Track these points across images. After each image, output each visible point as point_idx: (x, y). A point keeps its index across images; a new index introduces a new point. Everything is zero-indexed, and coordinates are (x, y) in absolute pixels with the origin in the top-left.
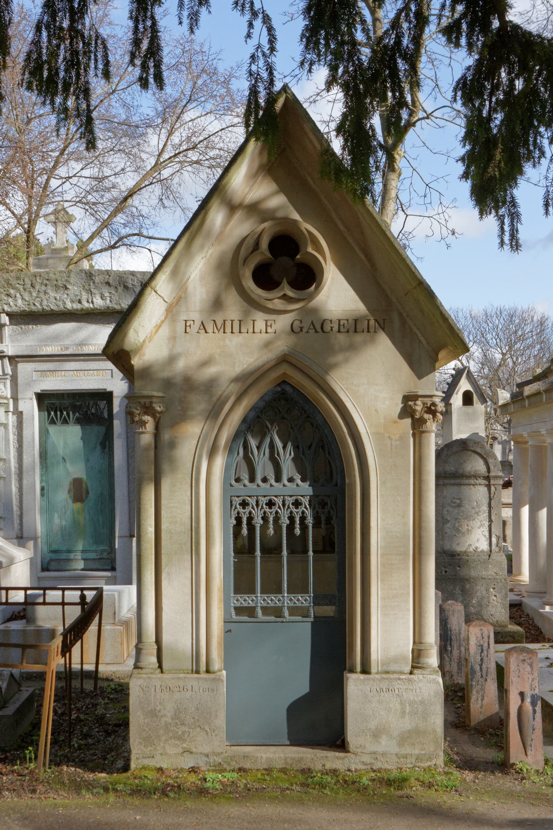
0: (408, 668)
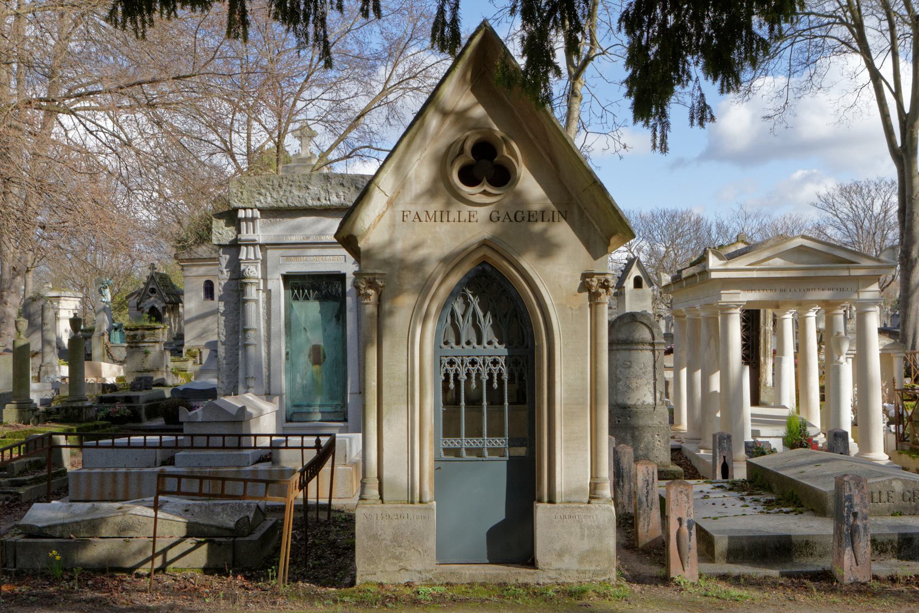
0: (587, 499)
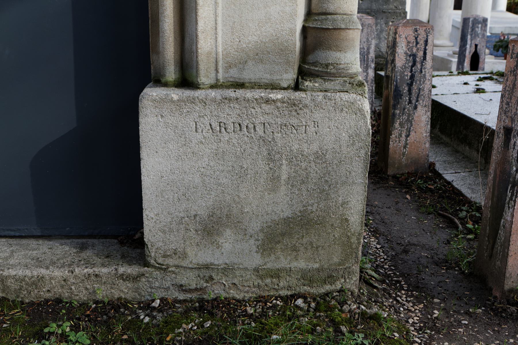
0: (290, 76)
